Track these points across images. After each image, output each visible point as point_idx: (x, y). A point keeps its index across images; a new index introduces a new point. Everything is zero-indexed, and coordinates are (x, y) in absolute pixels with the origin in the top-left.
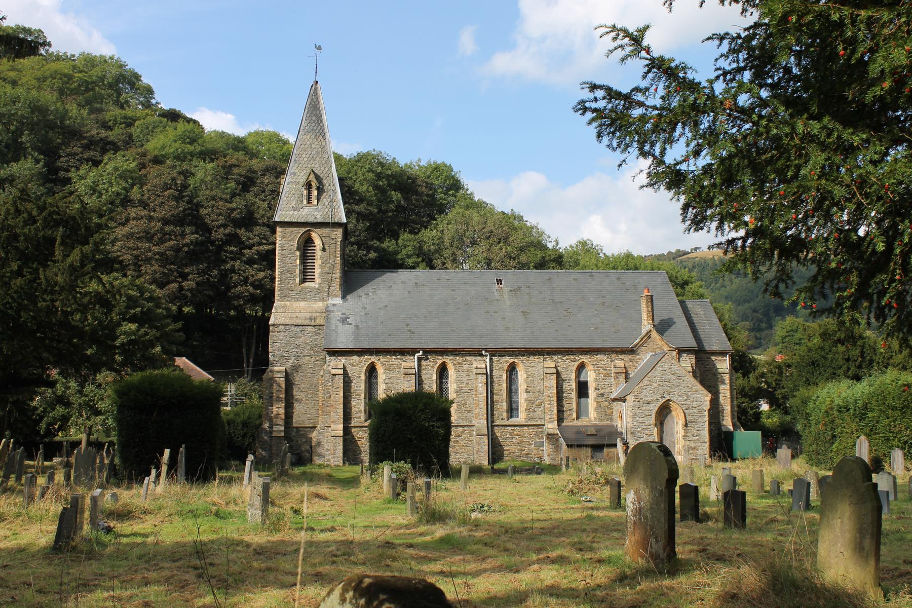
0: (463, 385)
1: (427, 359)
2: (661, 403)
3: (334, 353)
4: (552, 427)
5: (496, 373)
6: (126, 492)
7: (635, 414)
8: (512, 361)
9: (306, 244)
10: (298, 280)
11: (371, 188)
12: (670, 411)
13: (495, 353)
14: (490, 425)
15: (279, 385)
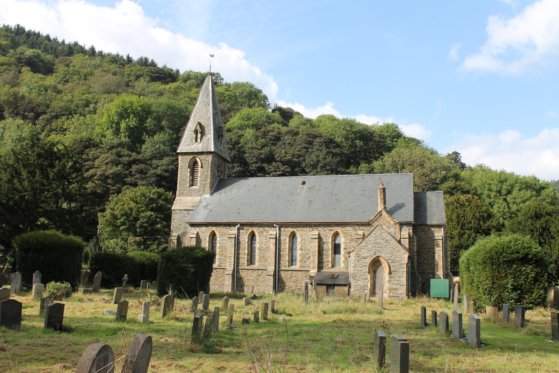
0: (263, 245)
1: (243, 229)
3: (193, 225)
4: (313, 272)
5: (282, 238)
6: (219, 306)
8: (292, 230)
9: (193, 166)
10: (188, 185)
11: (343, 139)
12: (381, 264)
13: (282, 225)
14: (277, 270)
15: (174, 243)
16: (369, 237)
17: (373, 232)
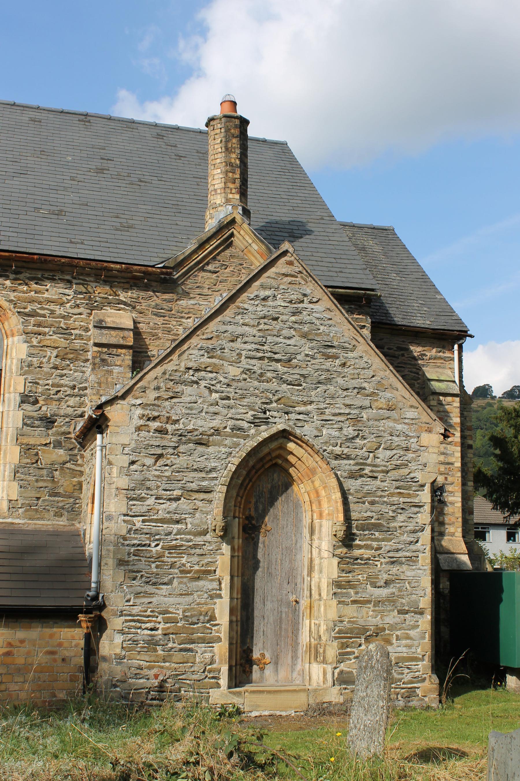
2: (252, 444)
7: (142, 483)
16: (229, 313)
17: (252, 291)
